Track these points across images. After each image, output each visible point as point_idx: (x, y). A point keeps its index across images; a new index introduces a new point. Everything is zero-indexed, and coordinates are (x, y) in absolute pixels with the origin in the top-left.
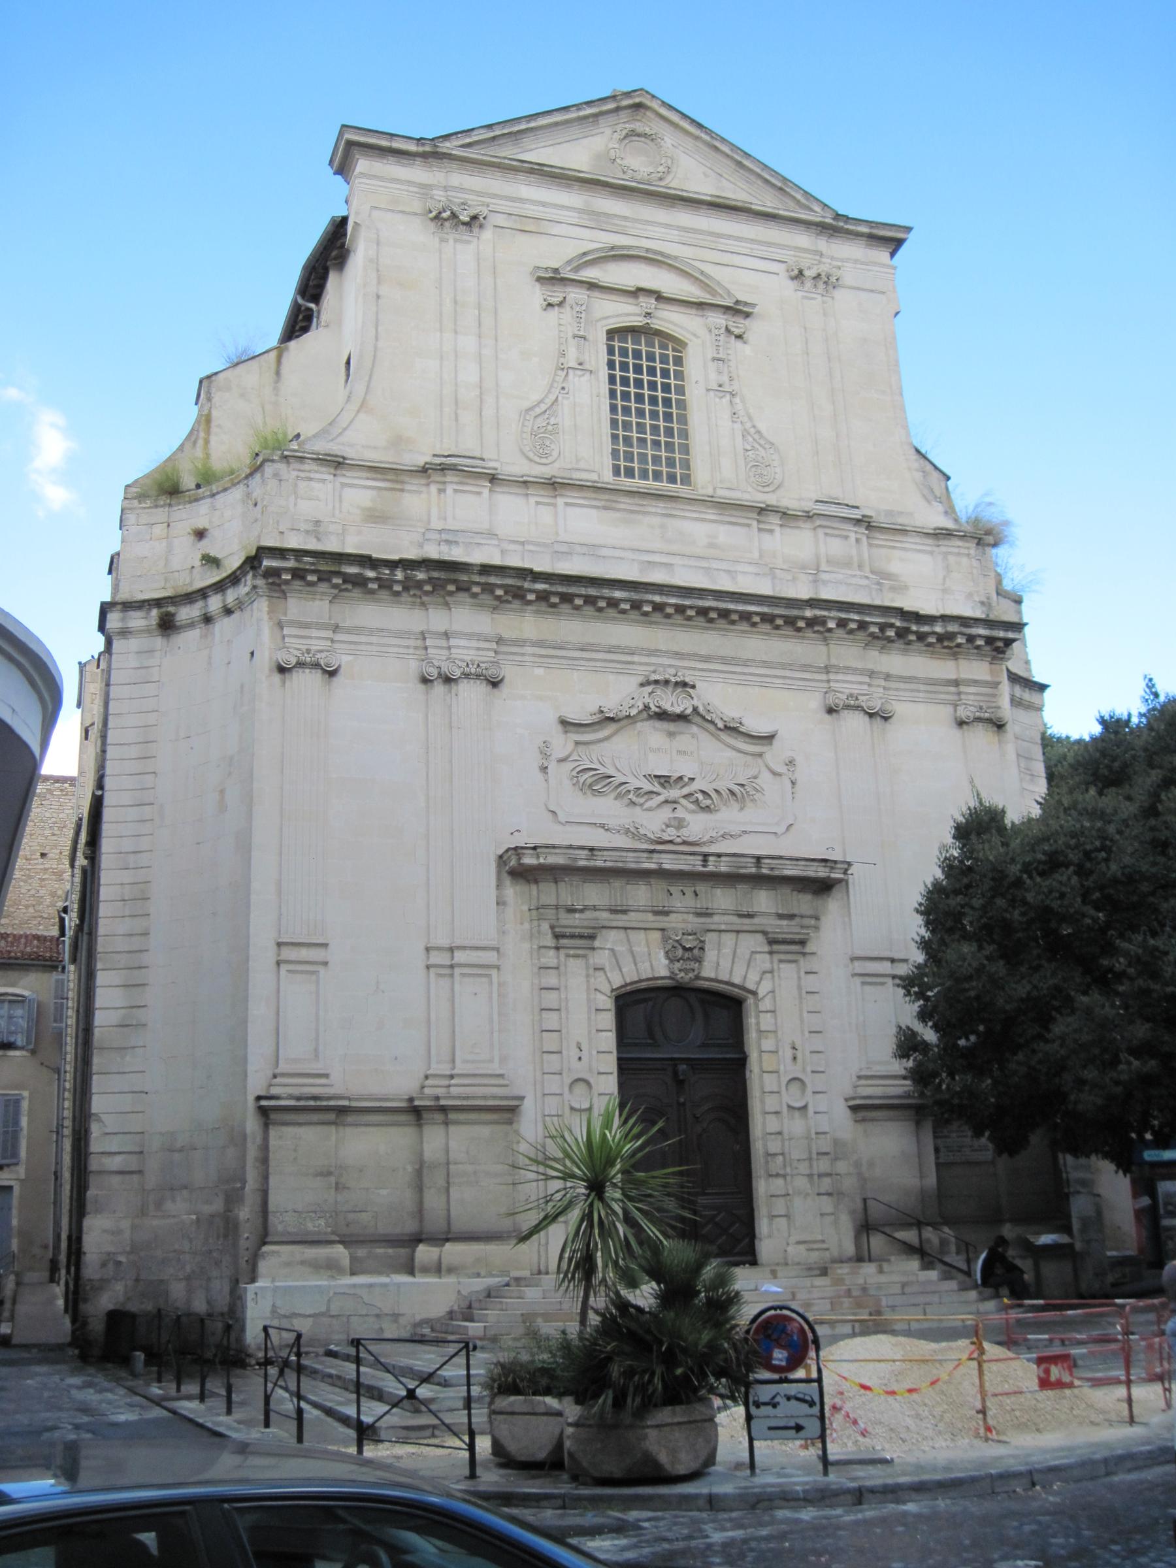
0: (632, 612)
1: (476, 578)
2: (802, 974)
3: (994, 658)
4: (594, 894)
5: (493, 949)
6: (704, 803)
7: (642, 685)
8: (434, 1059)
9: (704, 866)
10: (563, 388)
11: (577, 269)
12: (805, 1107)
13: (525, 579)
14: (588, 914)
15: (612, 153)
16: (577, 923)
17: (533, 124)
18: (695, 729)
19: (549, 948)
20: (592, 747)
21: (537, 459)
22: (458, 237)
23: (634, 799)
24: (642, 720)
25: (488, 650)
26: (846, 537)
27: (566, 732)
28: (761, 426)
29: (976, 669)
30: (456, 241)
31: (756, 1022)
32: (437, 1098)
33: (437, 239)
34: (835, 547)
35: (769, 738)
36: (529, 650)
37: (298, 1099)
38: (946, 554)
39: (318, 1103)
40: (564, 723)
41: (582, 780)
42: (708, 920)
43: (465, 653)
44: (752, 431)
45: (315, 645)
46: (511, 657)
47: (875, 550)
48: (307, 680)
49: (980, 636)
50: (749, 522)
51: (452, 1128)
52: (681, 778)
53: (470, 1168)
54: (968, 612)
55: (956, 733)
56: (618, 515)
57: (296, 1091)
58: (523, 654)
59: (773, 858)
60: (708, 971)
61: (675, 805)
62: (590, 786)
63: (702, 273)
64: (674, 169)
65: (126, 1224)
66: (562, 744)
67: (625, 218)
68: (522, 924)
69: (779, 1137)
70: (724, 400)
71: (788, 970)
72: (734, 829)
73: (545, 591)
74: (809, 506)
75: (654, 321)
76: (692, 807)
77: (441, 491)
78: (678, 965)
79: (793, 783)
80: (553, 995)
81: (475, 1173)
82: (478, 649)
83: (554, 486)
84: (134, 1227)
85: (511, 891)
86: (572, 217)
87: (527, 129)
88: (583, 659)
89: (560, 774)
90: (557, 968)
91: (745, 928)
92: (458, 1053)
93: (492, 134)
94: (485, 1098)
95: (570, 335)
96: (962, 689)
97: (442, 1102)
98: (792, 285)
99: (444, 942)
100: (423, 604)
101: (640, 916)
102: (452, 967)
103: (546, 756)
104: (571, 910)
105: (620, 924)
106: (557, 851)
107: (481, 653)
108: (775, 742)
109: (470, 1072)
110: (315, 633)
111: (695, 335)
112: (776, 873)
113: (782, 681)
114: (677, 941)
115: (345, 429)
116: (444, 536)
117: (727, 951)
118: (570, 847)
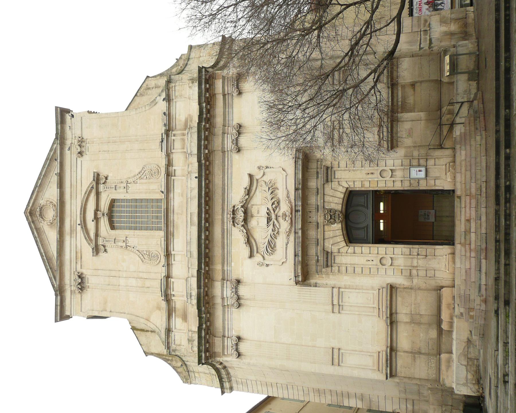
0: (209, 148)
1: (202, 290)
2: (339, 169)
3: (213, 78)
4: (312, 251)
5: (332, 290)
6: (277, 204)
7: (235, 226)
8: (373, 314)
9: (299, 212)
10: (133, 248)
11: (91, 240)
12: (391, 170)
13: (201, 272)
14: (319, 254)
15: (49, 224)
16: (322, 258)
17: (44, 254)
20: (258, 247)
21: (159, 259)
22: (86, 282)
23: (276, 232)
24: (248, 226)
25: (227, 283)
26: (174, 140)
27: (254, 256)
28: (137, 171)
29: (219, 84)
30: (88, 283)
31: (358, 186)
32: (387, 317)
33: (88, 289)
34: (178, 145)
35: (251, 176)
36: (226, 268)
37: (387, 366)
38: (176, 97)
39: (389, 360)
40: (251, 256)
41: (270, 252)
42: (320, 207)
43: (228, 292)
44: (139, 175)
45: (230, 344)
46: (229, 274)
47: (178, 127)
48: (242, 347)
49: (205, 87)
50: (172, 180)
51: (398, 312)
52: (267, 213)
54: (196, 89)
55: (244, 96)
56: (175, 231)
57: (385, 365)
58: (227, 270)
59: (295, 184)
60: (339, 207)
61: (278, 215)
62: (272, 248)
63: (85, 193)
64: (51, 200)
65: (432, 407)
66: (258, 258)
67: (71, 221)
68: (323, 277)
69: (403, 181)
70: (130, 186)
71: (338, 175)
72: (285, 193)
73: (204, 265)
74: (164, 154)
75: (105, 212)
76: (278, 209)
77: (174, 295)
78: (337, 220)
79: (267, 167)
80: (349, 269)
81: (415, 304)
82: (227, 287)
83: (168, 255)
84: (433, 404)
85: (312, 281)
86: (73, 239)
87: (46, 256)
88: (227, 248)
89: (269, 259)
90: (339, 267)
91: (322, 192)
92: (370, 306)
93: (50, 270)
94: (387, 300)
95: (114, 244)
96: (226, 93)
97: (389, 316)
98: (85, 156)
99: (330, 307)
100: (213, 305)
101: (319, 234)
102: (339, 305)
103: (263, 265)
104: (318, 261)
105: (322, 242)
106: (296, 269)
107: (228, 286)
108: (252, 173)
109: (377, 302)
110: (226, 344)
111: (108, 196)
112: (301, 181)
113: (229, 170)
114: (328, 221)
115: (156, 326)
116: (189, 297)
117: (331, 199)
118: (295, 264)
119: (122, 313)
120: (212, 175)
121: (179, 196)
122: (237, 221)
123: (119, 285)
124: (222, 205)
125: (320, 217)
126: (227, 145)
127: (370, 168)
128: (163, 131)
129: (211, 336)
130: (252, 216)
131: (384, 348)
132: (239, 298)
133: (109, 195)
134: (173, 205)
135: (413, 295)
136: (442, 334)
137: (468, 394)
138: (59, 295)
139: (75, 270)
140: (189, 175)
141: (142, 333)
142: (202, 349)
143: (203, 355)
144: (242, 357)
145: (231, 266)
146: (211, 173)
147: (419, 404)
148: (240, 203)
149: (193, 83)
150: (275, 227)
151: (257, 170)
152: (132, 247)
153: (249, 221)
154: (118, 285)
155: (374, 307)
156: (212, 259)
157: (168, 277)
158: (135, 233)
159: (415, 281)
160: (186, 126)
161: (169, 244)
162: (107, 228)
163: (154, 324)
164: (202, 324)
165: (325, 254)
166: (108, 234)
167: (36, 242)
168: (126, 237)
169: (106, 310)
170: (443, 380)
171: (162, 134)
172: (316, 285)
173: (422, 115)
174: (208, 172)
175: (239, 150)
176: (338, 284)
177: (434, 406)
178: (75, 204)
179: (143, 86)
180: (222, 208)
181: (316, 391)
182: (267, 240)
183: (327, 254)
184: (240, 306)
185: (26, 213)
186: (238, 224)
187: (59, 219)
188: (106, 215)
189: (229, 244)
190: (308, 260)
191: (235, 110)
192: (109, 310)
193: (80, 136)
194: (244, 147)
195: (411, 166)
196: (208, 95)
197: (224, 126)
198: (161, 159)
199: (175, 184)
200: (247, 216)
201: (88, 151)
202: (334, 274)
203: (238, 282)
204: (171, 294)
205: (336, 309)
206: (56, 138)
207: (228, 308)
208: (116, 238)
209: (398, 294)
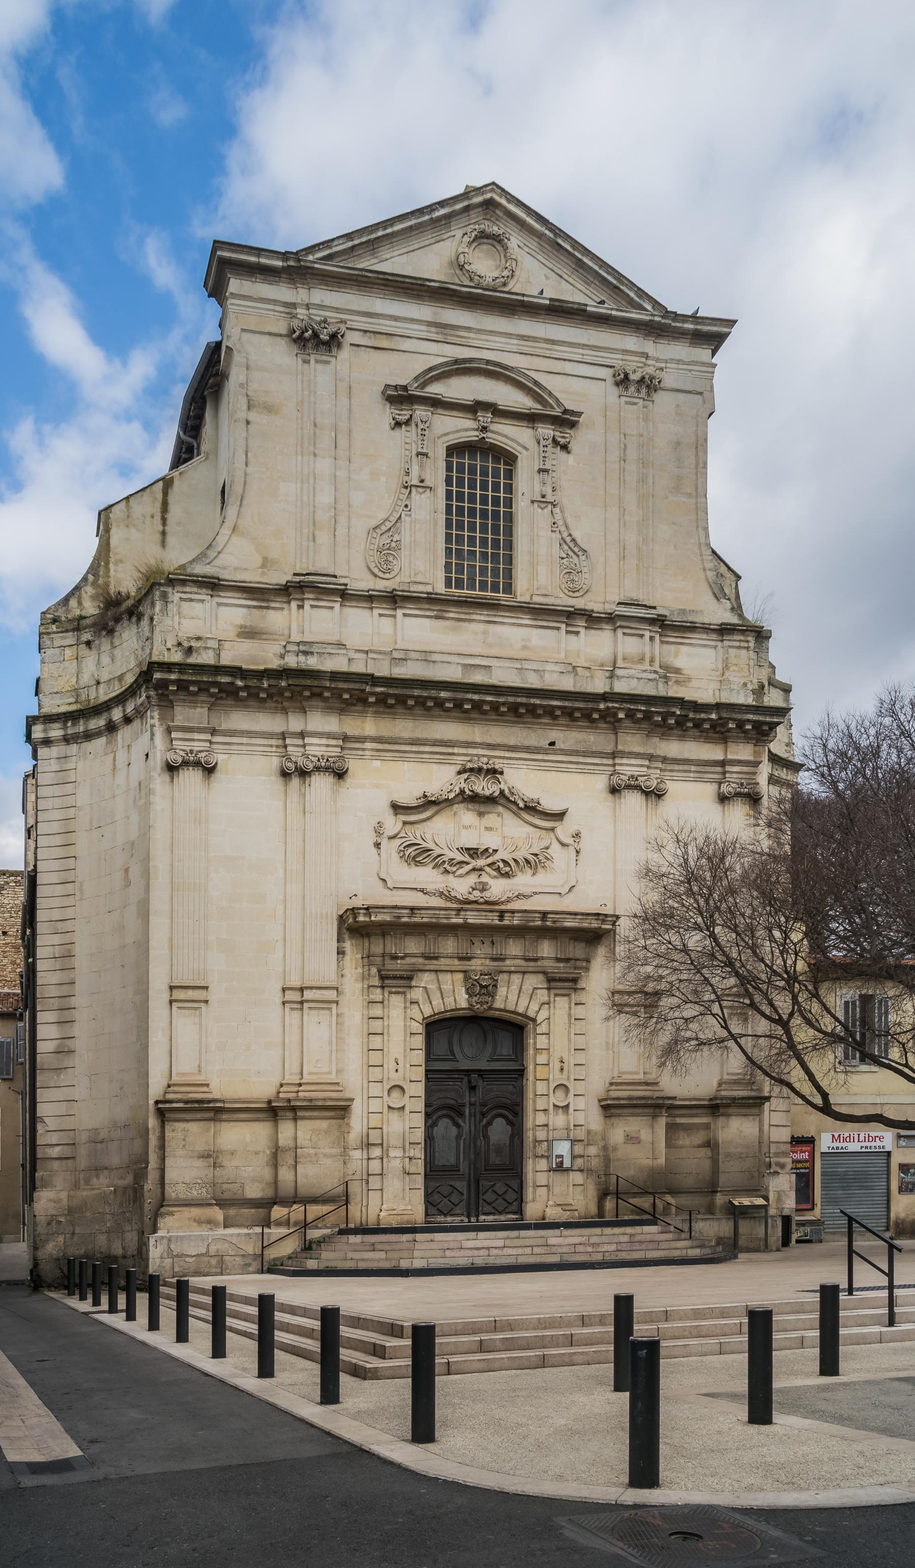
1: (328, 684)
2: (573, 1005)
4: (413, 946)
5: (333, 988)
7: (459, 773)
11: (424, 385)
12: (567, 1106)
13: (367, 683)
14: (408, 960)
15: (462, 258)
20: (416, 826)
22: (319, 357)
23: (448, 868)
24: (458, 803)
25: (336, 746)
26: (642, 636)
27: (396, 814)
28: (576, 534)
29: (742, 751)
33: (300, 360)
35: (560, 816)
36: (368, 745)
37: (186, 1102)
40: (397, 808)
41: (407, 854)
42: (501, 963)
43: (318, 749)
44: (568, 539)
45: (197, 746)
47: (666, 647)
48: (191, 778)
50: (330, 604)
52: (486, 850)
53: (312, 1151)
56: (448, 623)
58: (364, 750)
60: (499, 1004)
62: (414, 858)
63: (536, 383)
65: (64, 1195)
66: (392, 824)
67: (469, 329)
68: (356, 968)
70: (545, 510)
71: (562, 1003)
72: (527, 890)
73: (382, 693)
74: (611, 608)
75: (489, 434)
76: (494, 873)
77: (301, 607)
78: (475, 999)
79: (578, 852)
81: (316, 1154)
82: (328, 746)
85: (348, 945)
87: (383, 236)
89: (391, 849)
91: (530, 969)
93: (350, 244)
94: (324, 1099)
95: (414, 452)
96: (728, 768)
98: (615, 391)
101: (448, 961)
102: (302, 1003)
104: (394, 958)
105: (432, 967)
110: (197, 736)
112: (558, 925)
113: (575, 766)
114: (476, 980)
115: (219, 553)
116: (302, 648)
117: (515, 987)
118: (396, 907)
119: (247, 455)
120: (567, 726)
121: (523, 640)
122: (473, 778)
123: (315, 455)
125: (482, 965)
126: (627, 765)
127: (572, 1065)
128: (661, 611)
129: (213, 700)
130: (481, 814)
131: (216, 1095)
132: (303, 773)
133: (527, 449)
134: (503, 623)
135: (334, 1151)
136: (258, 1208)
137: (151, 1260)
138: (285, 264)
139: (349, 325)
140: (570, 668)
141: (158, 504)
142: (186, 673)
143: (173, 677)
144: (166, 777)
145: (373, 758)
146: (571, 723)
147: (67, 1171)
148: (509, 789)
149: (754, 691)
151: (573, 829)
152: (407, 503)
153: (470, 806)
154: (317, 452)
155: (302, 1074)
156: (389, 713)
157: (344, 595)
158: (440, 515)
159: (357, 1154)
160: (668, 672)
161: (419, 606)
162: (451, 437)
163: (225, 546)
164: (245, 678)
166: (439, 438)
167: (420, 211)
168: (431, 488)
169: (249, 408)
170: (171, 1214)
171: (654, 608)
172: (341, 952)
173: (662, 1161)
174: (391, 701)
175: (614, 790)
176: (344, 1000)
177: (66, 1200)
178: (509, 348)
179: (722, 564)
180: (499, 745)
181: (69, 950)
182: (431, 845)
183: (406, 979)
184: (285, 774)
185: (492, 190)
186: (465, 780)
187: (478, 294)
188: (483, 435)
189: (419, 756)
190: (396, 938)
191: (691, 786)
192: (252, 416)
193: (662, 385)
194: (620, 803)
195: (574, 1142)
196: (730, 726)
197: (665, 760)
198: (602, 600)
199: (549, 632)
200: (484, 802)
201: (627, 403)
202: (366, 992)
203: (340, 775)
204: (303, 600)
205: (291, 995)
206: (666, 313)
207: (277, 746)
208: (428, 460)
209: (334, 1122)
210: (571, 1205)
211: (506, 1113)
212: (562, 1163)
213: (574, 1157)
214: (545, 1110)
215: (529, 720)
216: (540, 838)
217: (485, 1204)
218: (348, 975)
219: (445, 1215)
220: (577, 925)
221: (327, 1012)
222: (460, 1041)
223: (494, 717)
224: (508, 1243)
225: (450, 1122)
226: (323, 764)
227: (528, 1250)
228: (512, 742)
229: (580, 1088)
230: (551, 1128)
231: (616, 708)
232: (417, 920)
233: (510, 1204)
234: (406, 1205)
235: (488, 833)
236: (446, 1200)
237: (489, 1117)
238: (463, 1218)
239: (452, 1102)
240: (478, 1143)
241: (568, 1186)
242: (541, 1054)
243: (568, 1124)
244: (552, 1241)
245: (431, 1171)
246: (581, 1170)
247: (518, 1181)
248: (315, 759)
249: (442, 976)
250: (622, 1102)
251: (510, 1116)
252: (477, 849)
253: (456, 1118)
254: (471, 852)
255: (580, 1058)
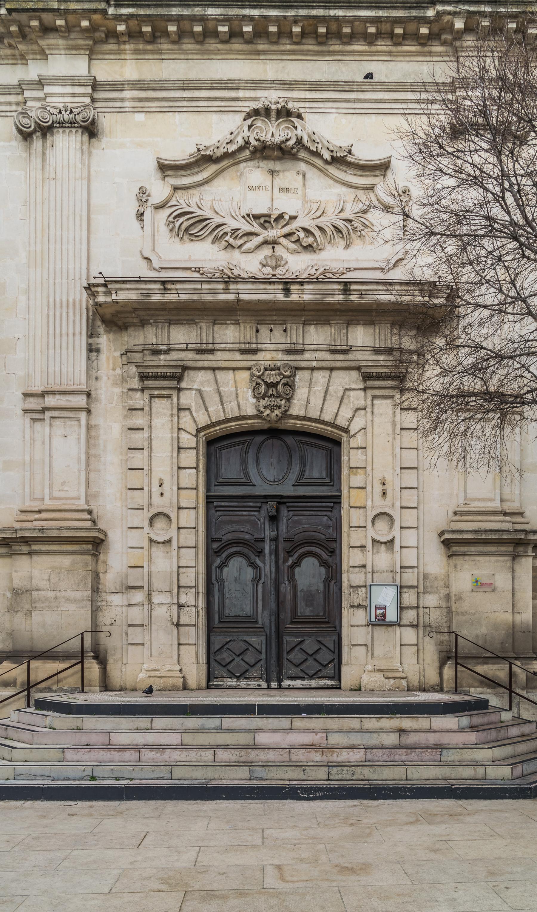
5: (80, 392)
12: (392, 541)
14: (174, 355)
16: (162, 363)
18: (302, 166)
19: (136, 390)
20: (190, 191)
23: (231, 241)
24: (246, 160)
25: (84, 95)
41: (177, 224)
42: (298, 357)
46: (111, 104)
52: (281, 217)
53: (51, 594)
58: (122, 100)
60: (297, 409)
62: (187, 230)
68: (114, 369)
76: (293, 246)
78: (263, 402)
81: (56, 598)
82: (73, 95)
91: (338, 364)
94: (59, 529)
104: (156, 352)
105: (206, 364)
107: (77, 99)
113: (399, 106)
117: (319, 388)
120: (390, 53)
124: (304, 82)
135: (79, 595)
145: (135, 111)
146: (394, 49)
150: (245, 239)
156: (153, 52)
165: (172, 370)
180: (296, 82)
182: (208, 213)
195: (401, 589)
209: (78, 558)
210: (397, 670)
211: (318, 550)
212: (384, 615)
213: (401, 608)
214: (363, 547)
215: (337, 48)
216: (356, 199)
217: (290, 665)
218: (105, 378)
219: (238, 678)
220: (392, 298)
221: (74, 423)
222: (257, 461)
223: (289, 47)
224: (188, 739)
225: (245, 562)
226: (66, 117)
227: (208, 755)
228: (316, 77)
229: (410, 518)
230: (369, 569)
231: (449, 13)
232: (173, 297)
233: (325, 666)
234: (174, 665)
235: (283, 195)
236: (238, 659)
237: (296, 555)
238: (260, 682)
239: (247, 537)
240: (282, 589)
241: (394, 646)
242: (356, 474)
243: (394, 565)
244: (262, 738)
245: (220, 622)
246: (415, 626)
247: (335, 638)
248: (56, 111)
249: (220, 375)
250: (465, 536)
251: (324, 555)
252: (269, 216)
253: (253, 557)
254: (262, 220)
255: (410, 478)
